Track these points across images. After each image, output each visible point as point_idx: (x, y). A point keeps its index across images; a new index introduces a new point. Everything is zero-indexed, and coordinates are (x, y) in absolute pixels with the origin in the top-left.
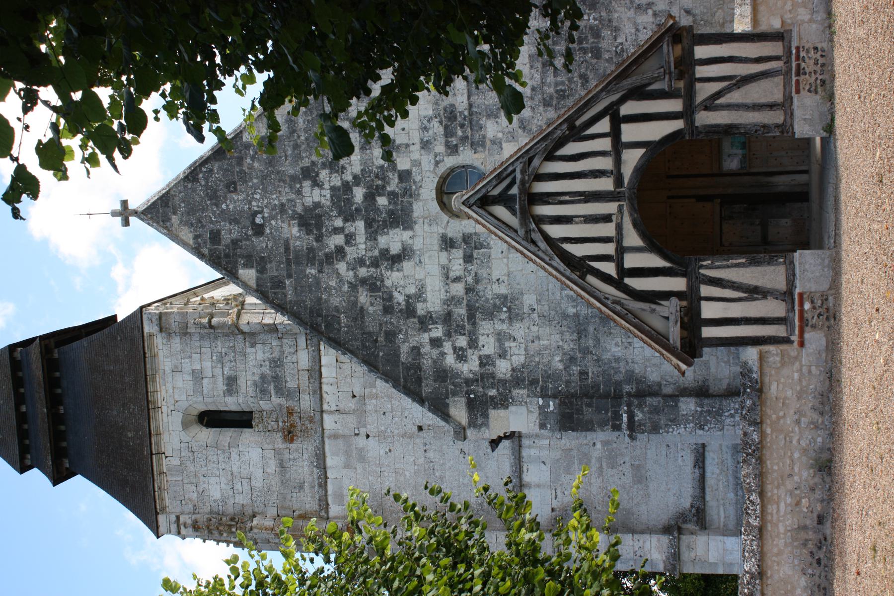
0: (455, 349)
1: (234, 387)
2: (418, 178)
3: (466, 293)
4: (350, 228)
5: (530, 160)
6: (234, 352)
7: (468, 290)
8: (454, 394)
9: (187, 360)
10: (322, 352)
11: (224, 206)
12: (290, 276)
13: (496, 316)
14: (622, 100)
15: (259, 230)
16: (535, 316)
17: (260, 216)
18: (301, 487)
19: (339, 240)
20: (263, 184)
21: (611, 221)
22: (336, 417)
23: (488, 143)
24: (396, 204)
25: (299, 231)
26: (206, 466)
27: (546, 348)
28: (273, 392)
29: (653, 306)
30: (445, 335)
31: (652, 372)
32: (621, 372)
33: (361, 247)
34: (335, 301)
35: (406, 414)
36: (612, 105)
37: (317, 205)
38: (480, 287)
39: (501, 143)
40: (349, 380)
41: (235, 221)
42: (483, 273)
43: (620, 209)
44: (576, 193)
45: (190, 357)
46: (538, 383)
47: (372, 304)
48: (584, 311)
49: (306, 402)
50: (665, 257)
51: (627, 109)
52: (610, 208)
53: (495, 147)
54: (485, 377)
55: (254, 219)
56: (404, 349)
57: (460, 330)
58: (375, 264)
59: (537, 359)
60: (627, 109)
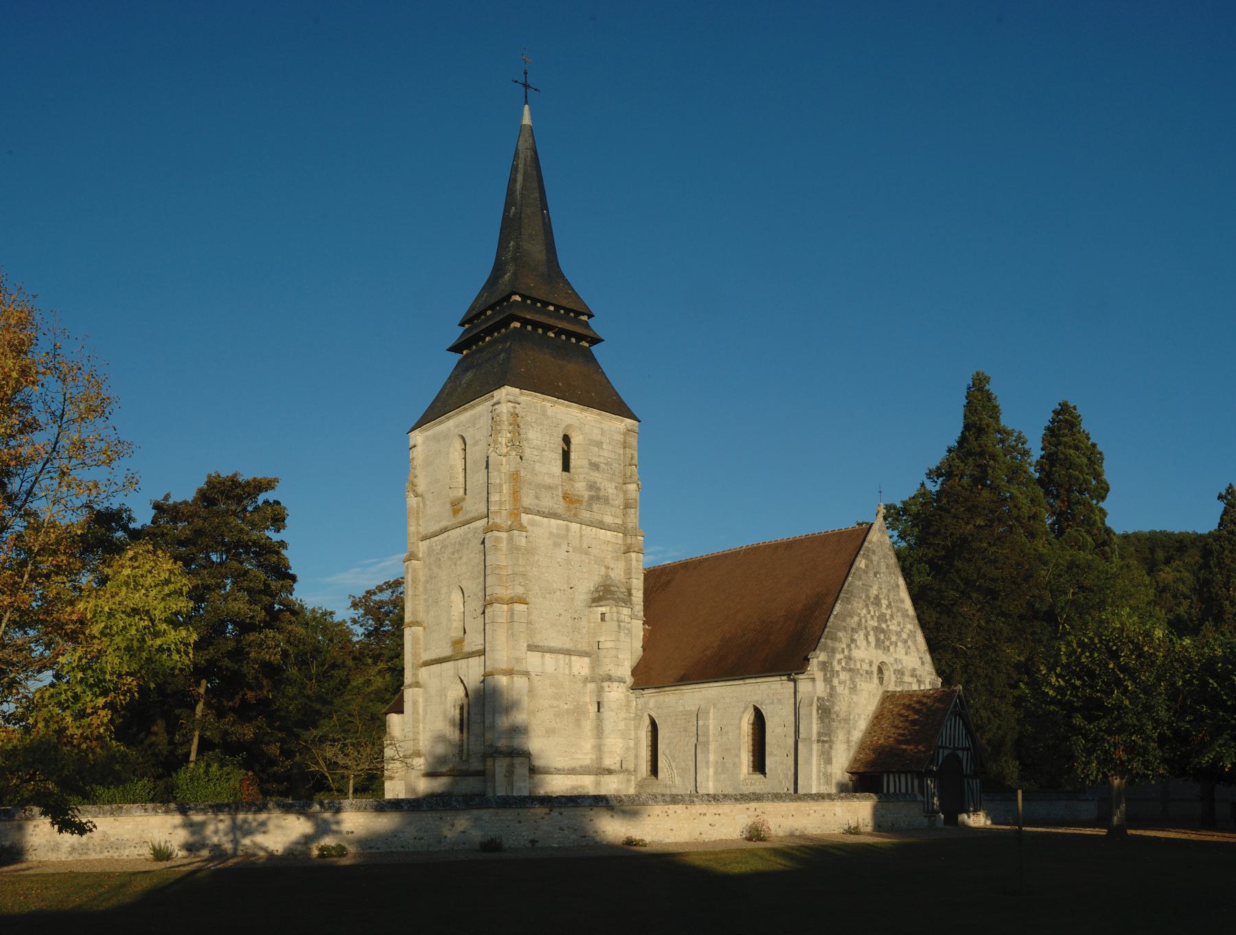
18: (537, 498)
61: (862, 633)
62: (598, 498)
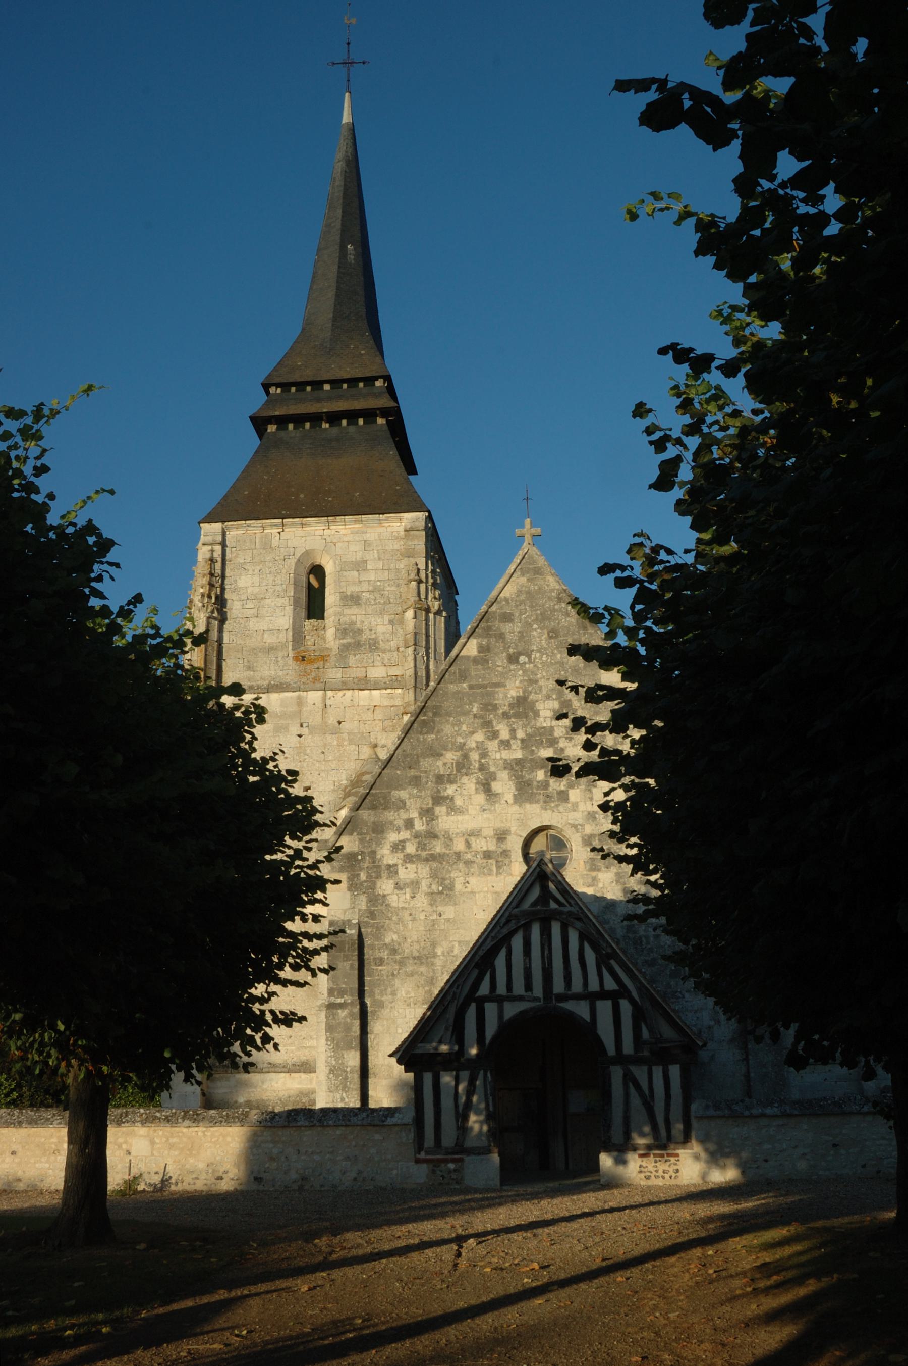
0: (404, 841)
1: (350, 603)
2: (561, 808)
3: (455, 853)
4: (516, 745)
5: (579, 919)
6: (384, 603)
7: (458, 855)
8: (362, 841)
9: (376, 556)
10: (384, 691)
11: (535, 626)
12: (471, 687)
13: (434, 879)
14: (632, 1001)
15: (513, 659)
16: (435, 917)
17: (527, 660)
18: (249, 668)
19: (505, 734)
20: (556, 663)
21: (526, 991)
22: (320, 705)
23: (594, 874)
24: (538, 788)
25: (513, 697)
26: (270, 573)
27: (405, 926)
28: (345, 641)
29: (451, 1028)
30: (417, 832)
31: (383, 1026)
32: (382, 996)
33: (498, 755)
34: (448, 730)
35: (323, 775)
36: (629, 992)
37: (537, 714)
38: (461, 865)
39: (592, 886)
40: (357, 717)
41: (522, 635)
42: (474, 869)
43: (536, 999)
44: (551, 960)
45: (379, 559)
46: (372, 919)
47: (445, 764)
48: (439, 962)
49: (334, 674)
50: (495, 1038)
51: (625, 1005)
52: (538, 990)
53: (590, 881)
54: (377, 870)
55: (523, 654)
56: (403, 794)
57: (421, 846)
58: (482, 768)
59: (394, 918)
60: (625, 1005)
61: (469, 784)
62: (358, 645)
